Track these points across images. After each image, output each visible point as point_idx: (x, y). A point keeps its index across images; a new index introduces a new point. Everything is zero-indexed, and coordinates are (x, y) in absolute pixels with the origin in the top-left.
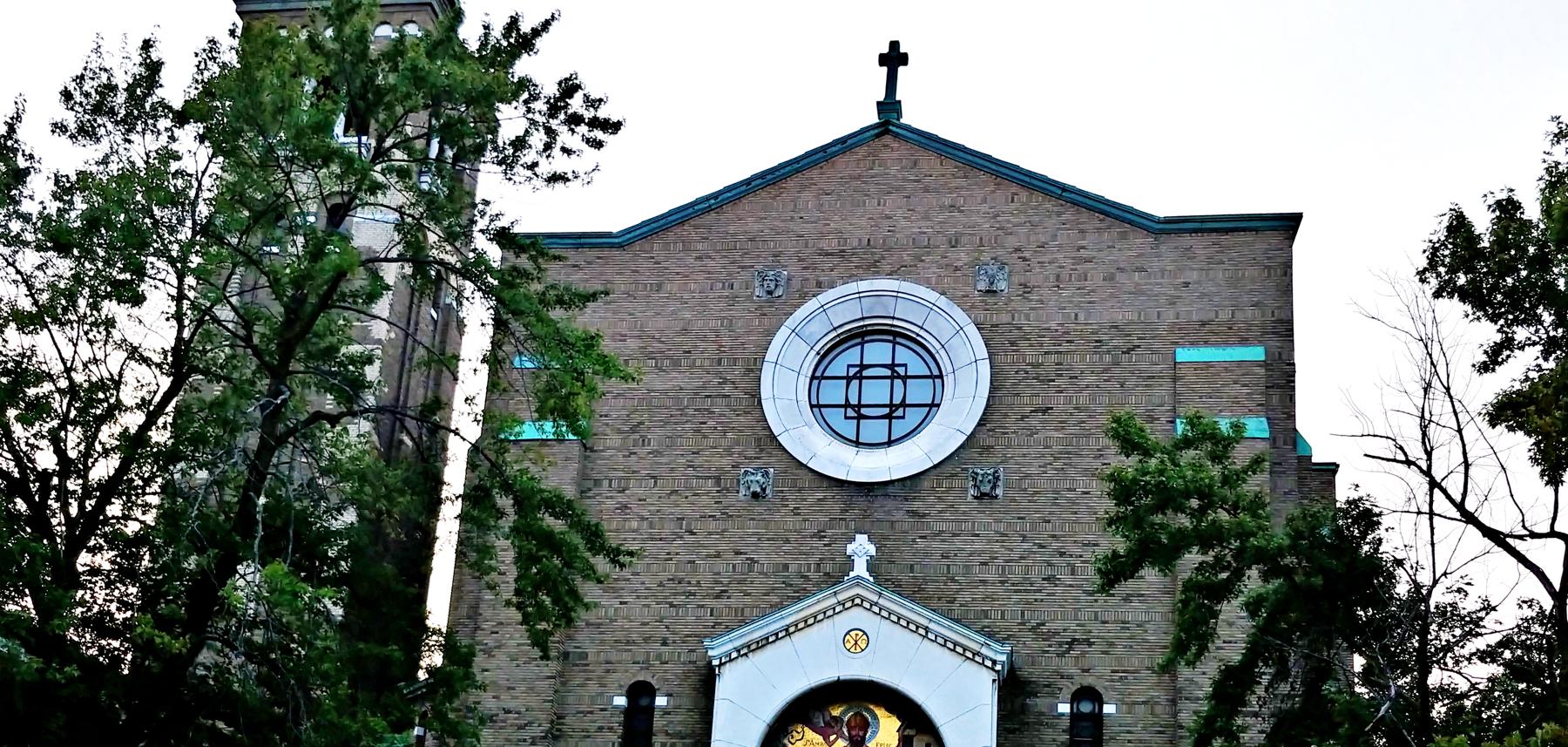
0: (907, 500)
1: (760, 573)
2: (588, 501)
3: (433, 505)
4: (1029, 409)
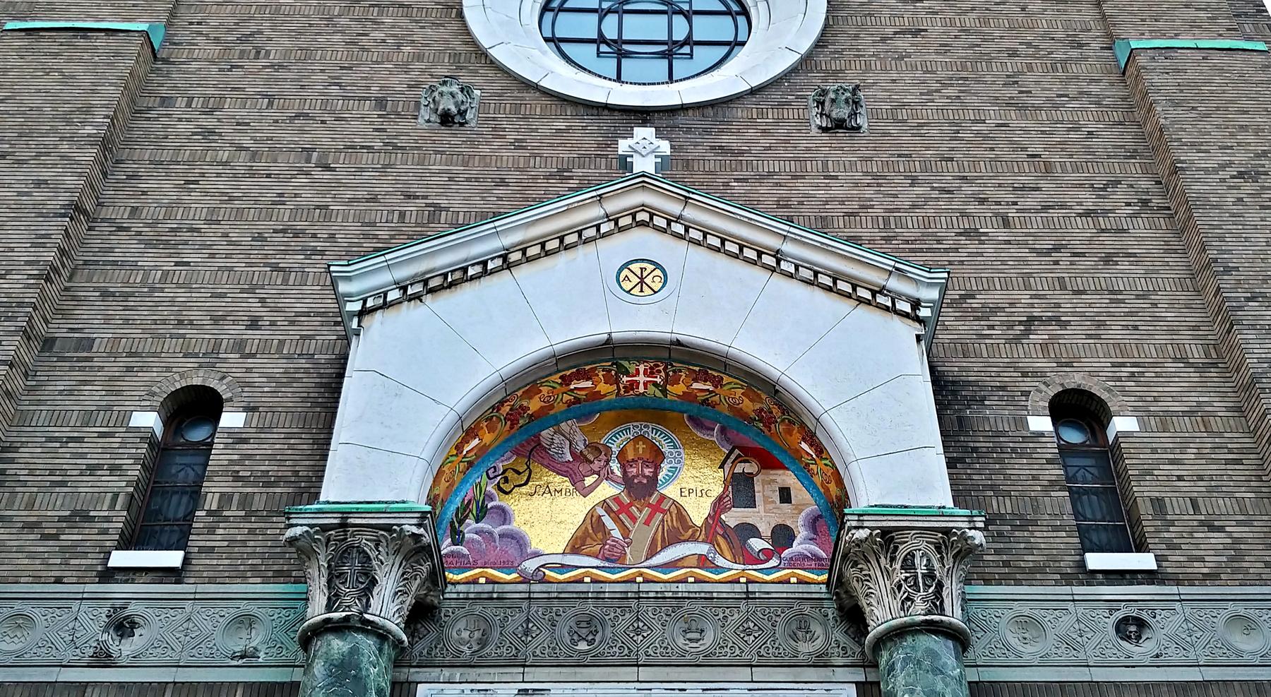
0: (710, 133)
1: (452, 225)
4: (890, 30)
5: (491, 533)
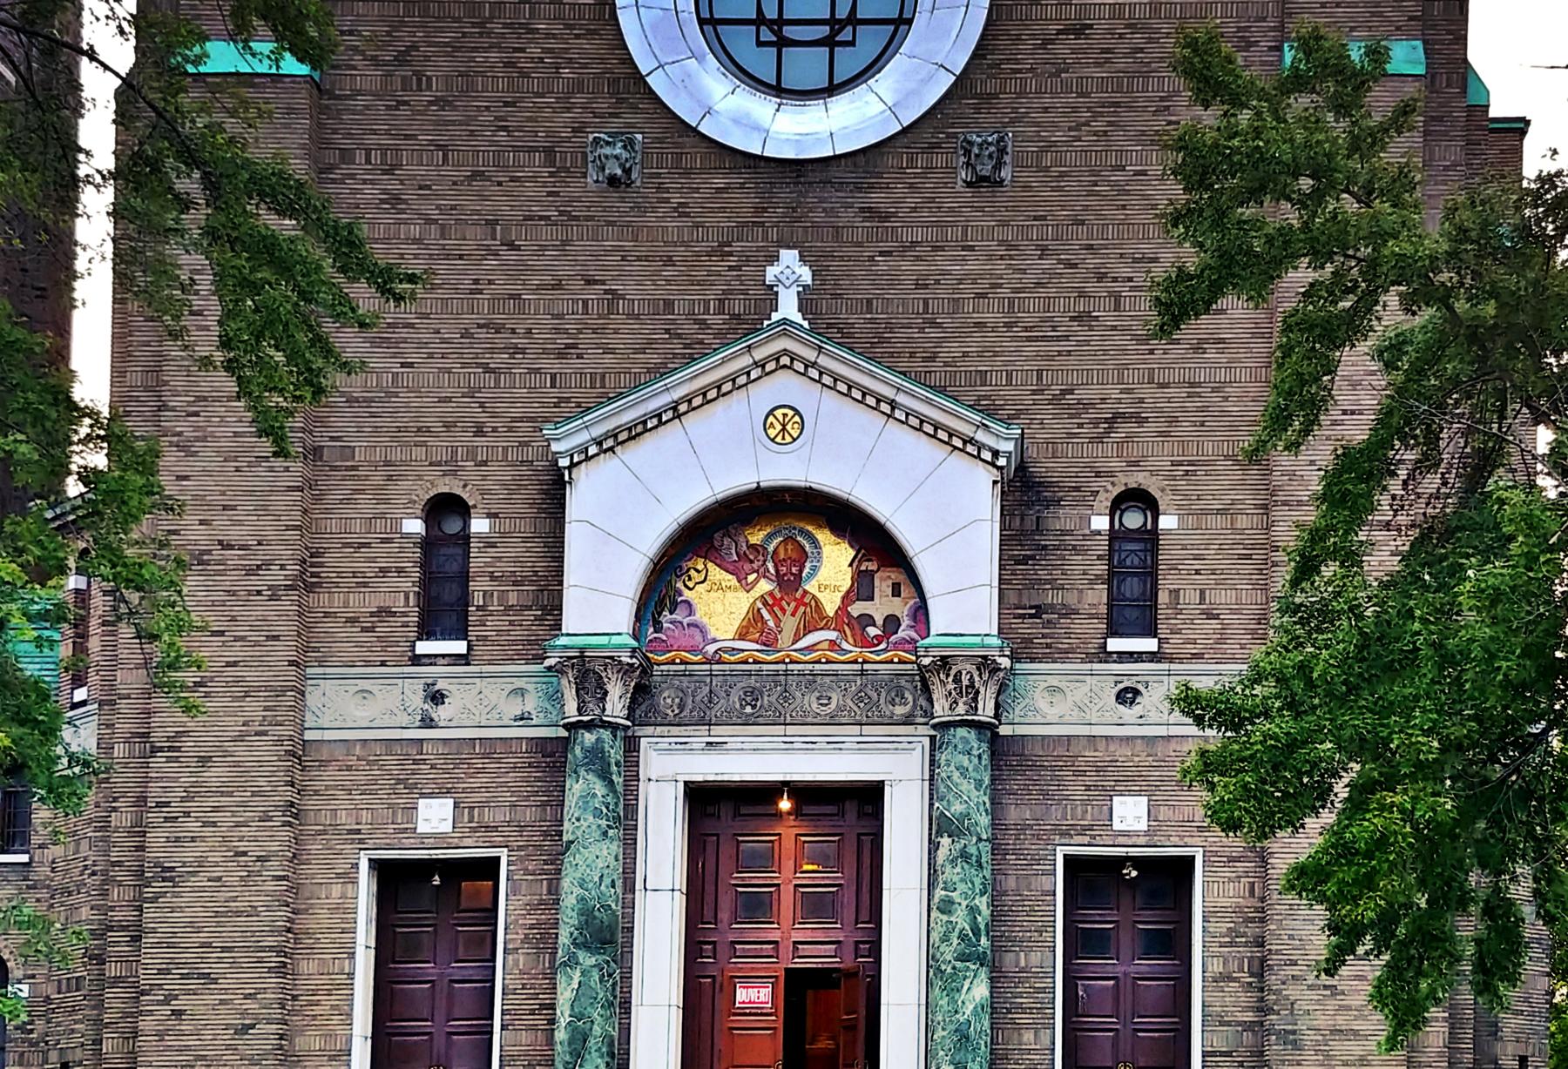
0: (860, 190)
2: (332, 189)
3: (65, 191)
5: (681, 623)
